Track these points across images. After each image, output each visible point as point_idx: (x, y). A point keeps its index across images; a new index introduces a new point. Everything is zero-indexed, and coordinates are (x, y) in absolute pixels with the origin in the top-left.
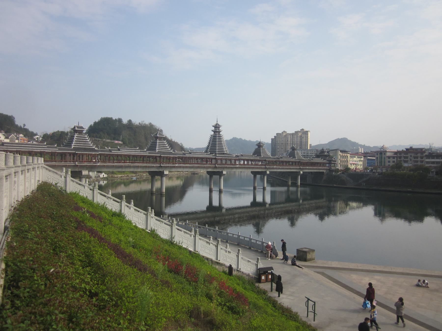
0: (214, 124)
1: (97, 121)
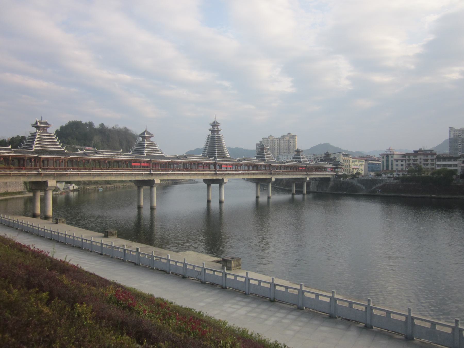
0: (212, 121)
1: (64, 125)
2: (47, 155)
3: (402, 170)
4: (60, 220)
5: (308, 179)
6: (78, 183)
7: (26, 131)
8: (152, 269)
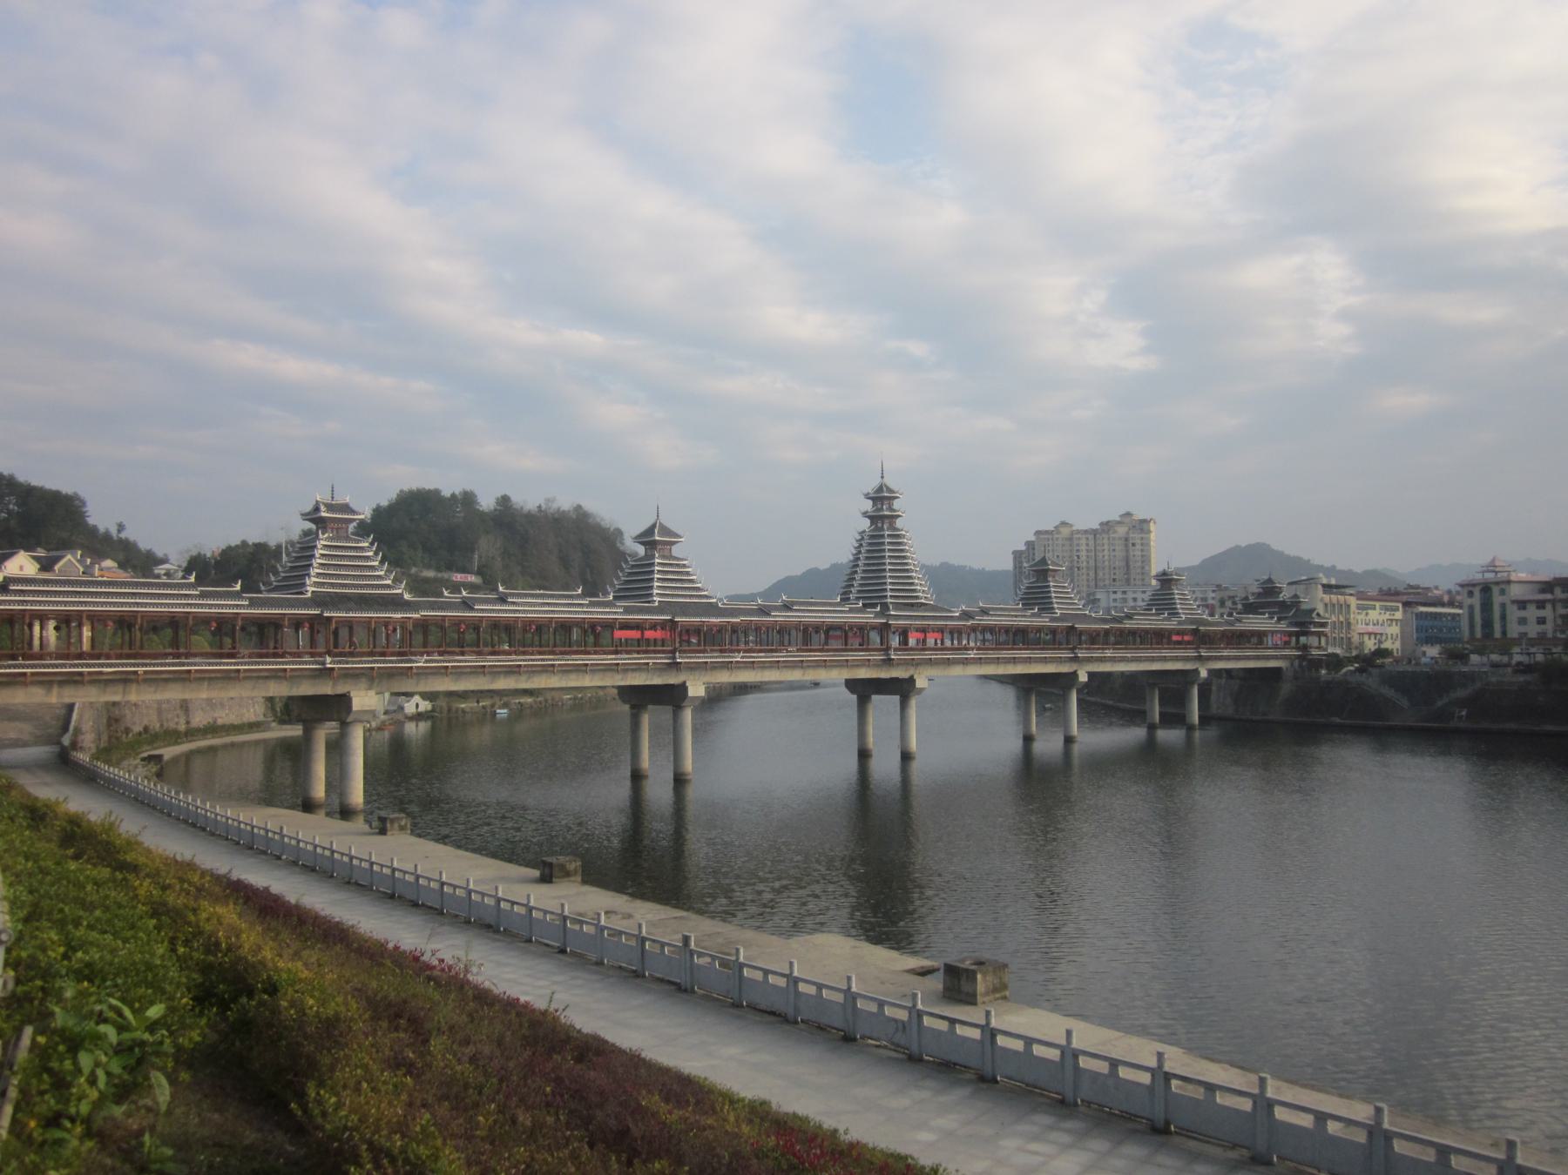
1: (385, 503)
2: (348, 610)
3: (1541, 639)
4: (392, 821)
5: (1204, 674)
6: (429, 696)
7: (277, 524)
8: (737, 1005)
